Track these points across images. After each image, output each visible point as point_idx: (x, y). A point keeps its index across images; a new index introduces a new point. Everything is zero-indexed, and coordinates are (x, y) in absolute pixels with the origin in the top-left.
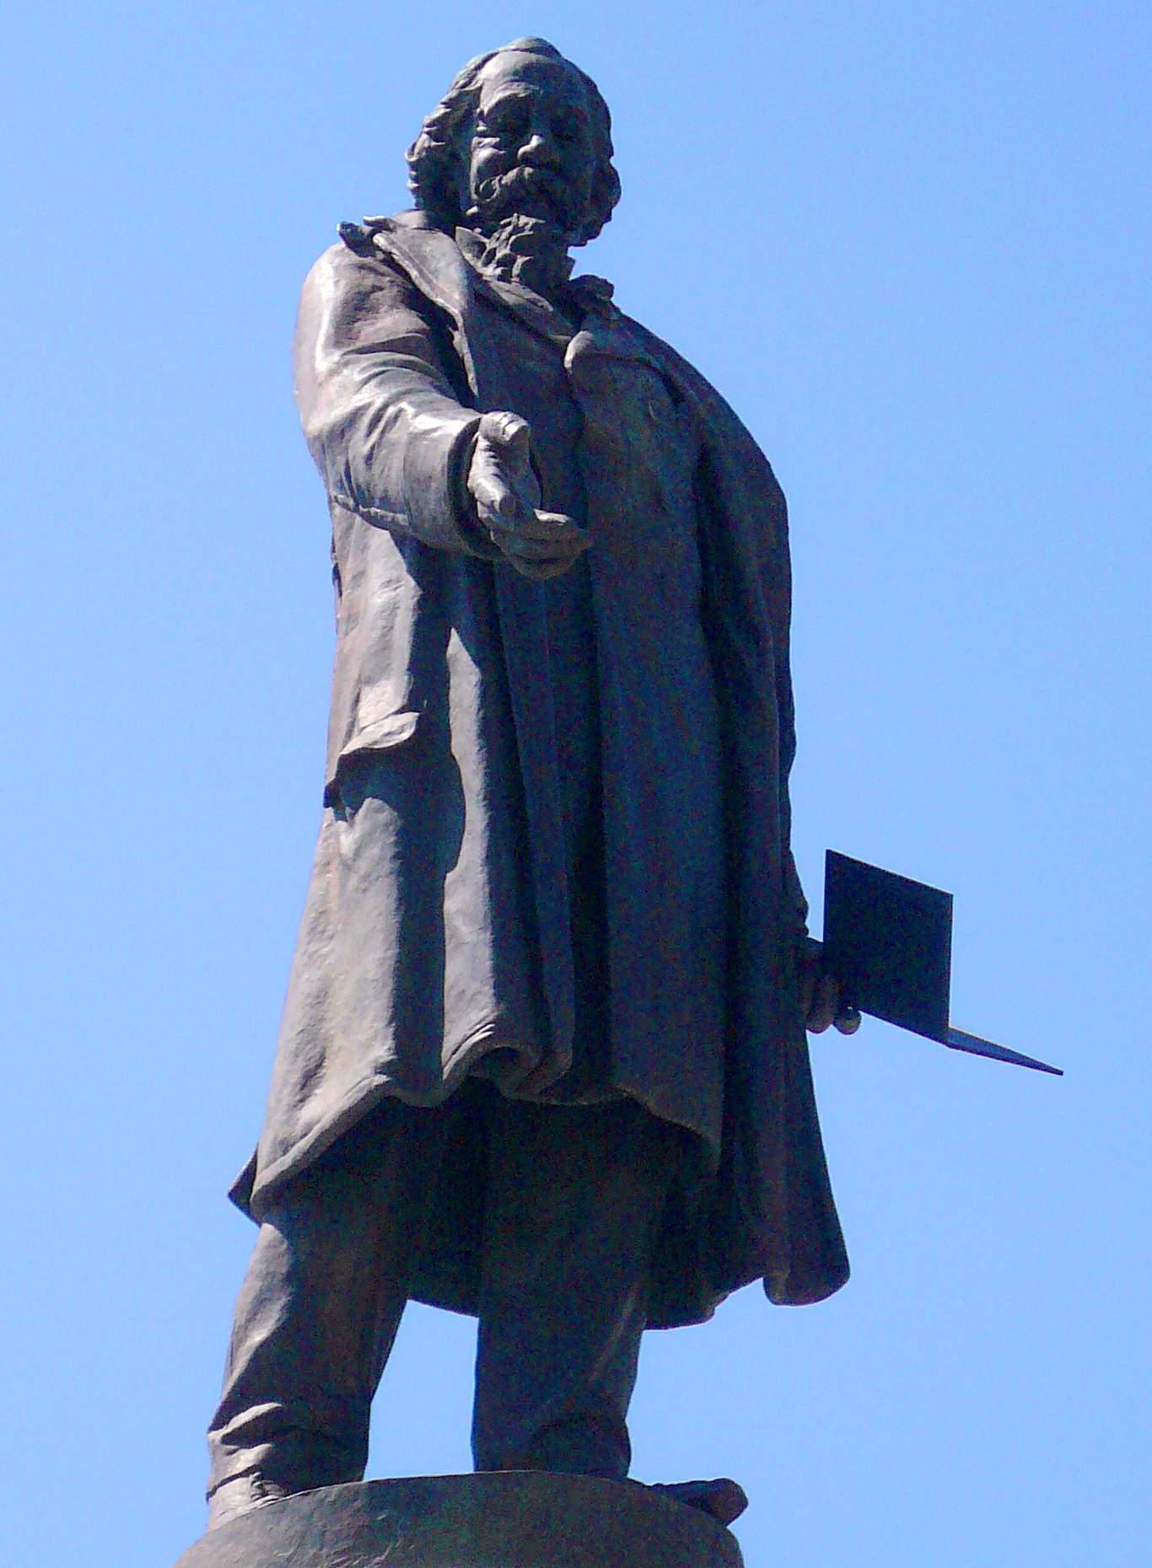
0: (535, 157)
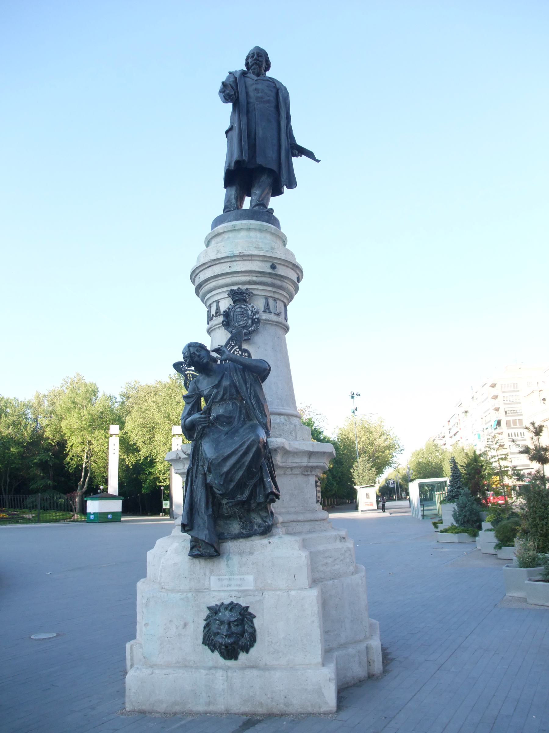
0: (259, 61)
